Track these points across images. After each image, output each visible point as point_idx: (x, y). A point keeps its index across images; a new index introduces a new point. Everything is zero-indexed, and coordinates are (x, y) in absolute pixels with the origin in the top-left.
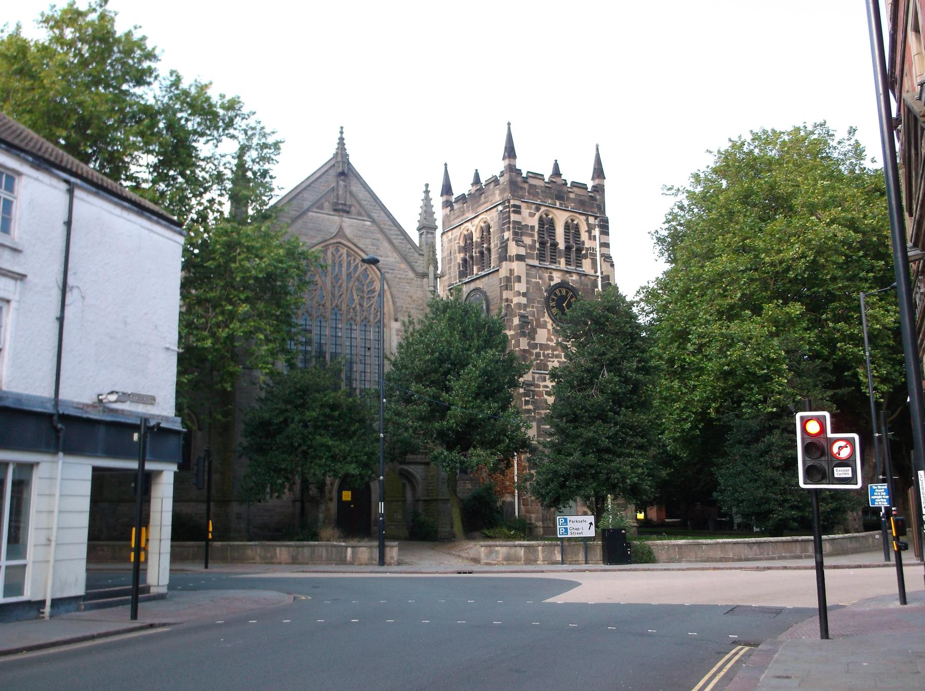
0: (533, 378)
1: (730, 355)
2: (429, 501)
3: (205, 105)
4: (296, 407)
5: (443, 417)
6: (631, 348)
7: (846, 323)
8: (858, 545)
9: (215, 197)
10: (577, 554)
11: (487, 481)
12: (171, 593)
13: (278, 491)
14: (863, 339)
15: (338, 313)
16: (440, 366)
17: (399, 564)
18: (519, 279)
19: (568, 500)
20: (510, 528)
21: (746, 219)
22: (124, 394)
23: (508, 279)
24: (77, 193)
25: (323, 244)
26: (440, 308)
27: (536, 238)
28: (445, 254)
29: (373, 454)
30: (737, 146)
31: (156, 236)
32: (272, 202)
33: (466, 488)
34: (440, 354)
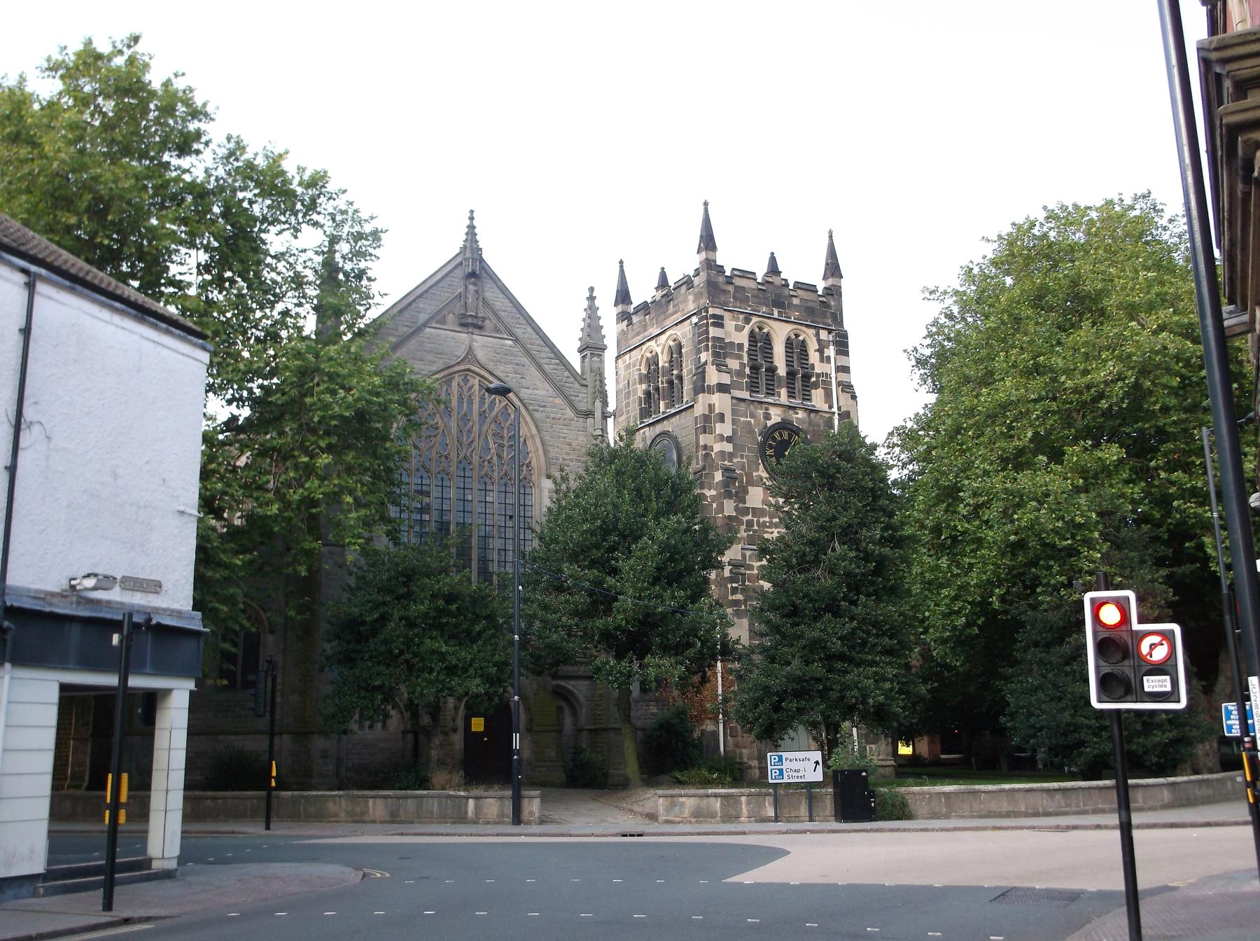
0: (744, 556)
1: (1018, 519)
2: (595, 730)
3: (278, 182)
4: (398, 598)
5: (608, 611)
6: (873, 510)
7: (1185, 472)
8: (1211, 792)
9: (290, 306)
10: (797, 807)
11: (679, 703)
12: (182, 868)
13: (370, 718)
14: (1208, 493)
15: (468, 467)
16: (604, 540)
17: (542, 822)
18: (721, 418)
19: (785, 729)
20: (711, 770)
21: (1039, 327)
22: (106, 577)
23: (706, 418)
24: (41, 287)
25: (446, 373)
26: (604, 458)
27: (745, 360)
28: (621, 386)
29: (506, 664)
30: (1024, 230)
31: (165, 352)
32: (373, 314)
33: (648, 713)
34: (604, 522)
